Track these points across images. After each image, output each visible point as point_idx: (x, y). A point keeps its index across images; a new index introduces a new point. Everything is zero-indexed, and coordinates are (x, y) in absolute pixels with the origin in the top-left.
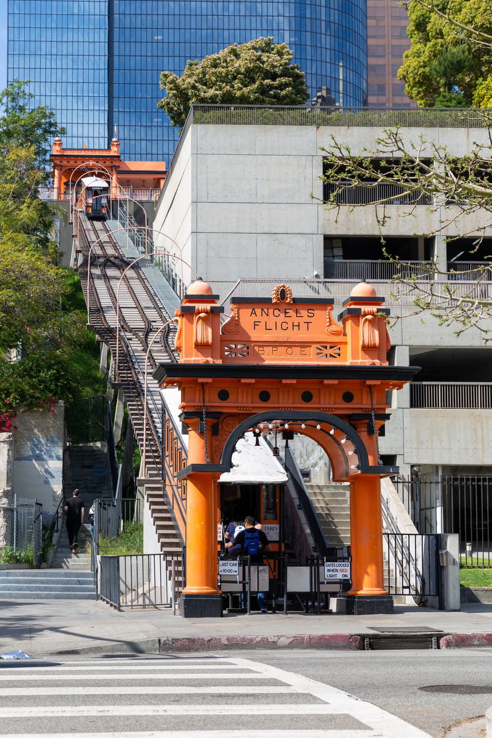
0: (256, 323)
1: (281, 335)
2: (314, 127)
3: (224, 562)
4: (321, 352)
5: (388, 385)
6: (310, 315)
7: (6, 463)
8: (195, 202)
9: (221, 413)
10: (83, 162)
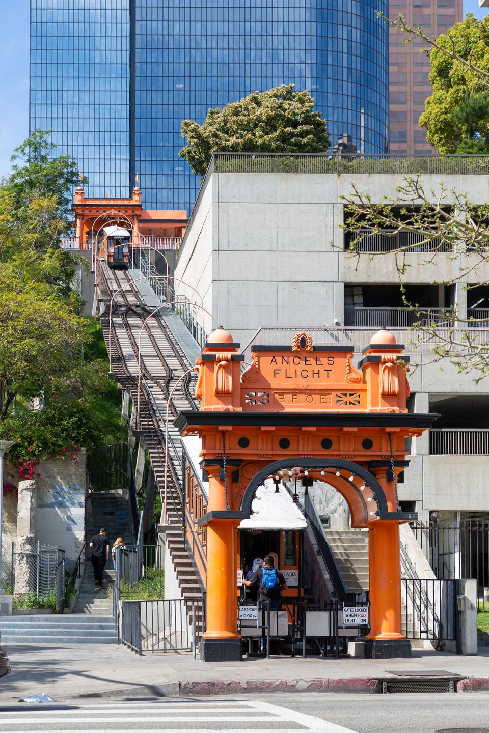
0: (276, 371)
1: (301, 383)
2: (335, 175)
3: (244, 607)
4: (341, 399)
5: (407, 432)
6: (330, 363)
7: (29, 510)
8: (216, 251)
9: (241, 460)
10: (105, 211)
